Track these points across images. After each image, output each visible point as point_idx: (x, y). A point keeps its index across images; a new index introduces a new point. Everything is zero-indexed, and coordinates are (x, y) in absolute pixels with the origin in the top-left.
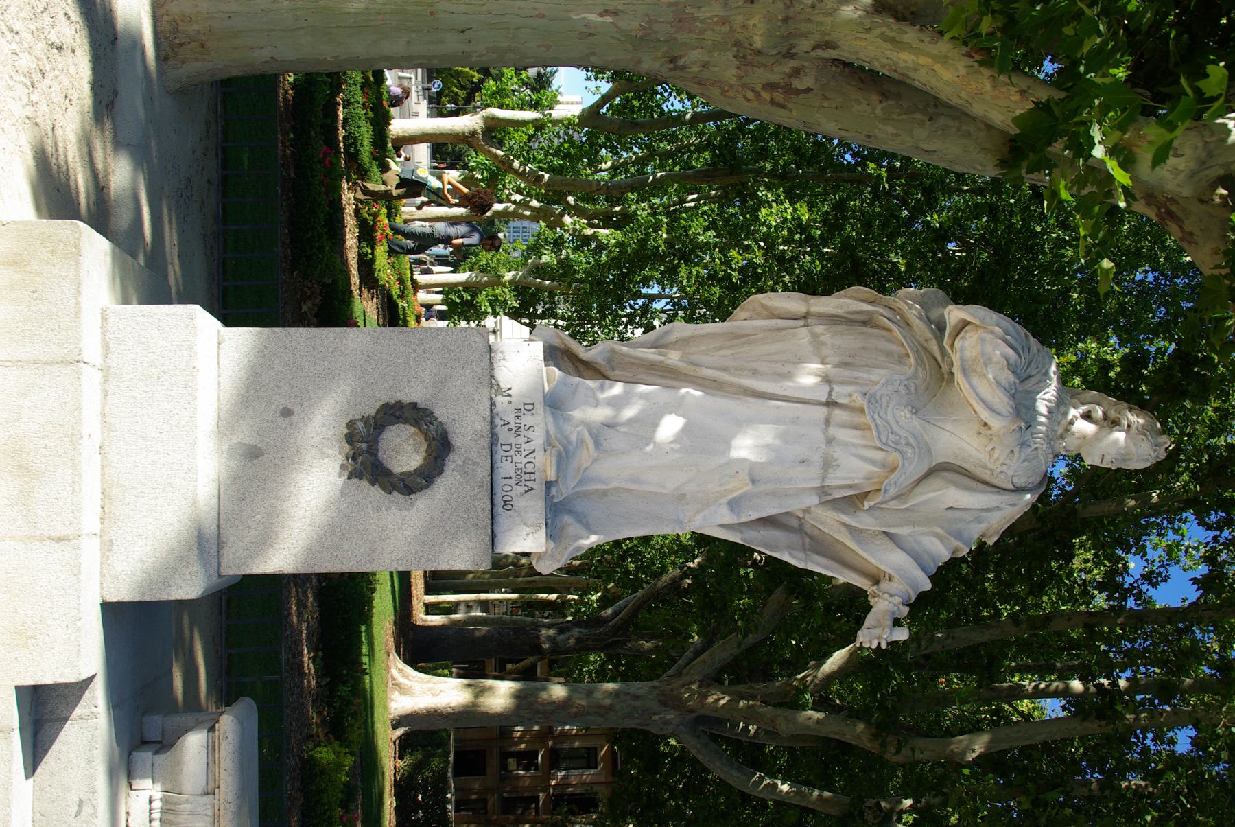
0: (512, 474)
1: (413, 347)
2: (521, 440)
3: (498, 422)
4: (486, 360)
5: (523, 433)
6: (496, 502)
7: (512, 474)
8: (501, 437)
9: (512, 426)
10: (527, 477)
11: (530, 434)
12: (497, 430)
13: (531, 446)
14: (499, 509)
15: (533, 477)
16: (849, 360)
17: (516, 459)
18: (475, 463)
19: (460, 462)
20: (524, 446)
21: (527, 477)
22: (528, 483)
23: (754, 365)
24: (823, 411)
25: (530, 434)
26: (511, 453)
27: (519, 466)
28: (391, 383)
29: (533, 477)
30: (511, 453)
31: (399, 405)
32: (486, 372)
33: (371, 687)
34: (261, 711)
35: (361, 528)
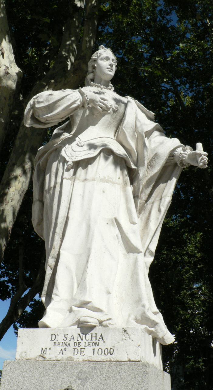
0: (92, 348)
2: (72, 343)
5: (68, 341)
7: (92, 348)
9: (63, 348)
11: (69, 337)
14: (113, 357)
15: (94, 335)
17: (83, 346)
19: (79, 382)
22: (98, 338)
26: (79, 348)
27: (87, 344)
30: (79, 348)
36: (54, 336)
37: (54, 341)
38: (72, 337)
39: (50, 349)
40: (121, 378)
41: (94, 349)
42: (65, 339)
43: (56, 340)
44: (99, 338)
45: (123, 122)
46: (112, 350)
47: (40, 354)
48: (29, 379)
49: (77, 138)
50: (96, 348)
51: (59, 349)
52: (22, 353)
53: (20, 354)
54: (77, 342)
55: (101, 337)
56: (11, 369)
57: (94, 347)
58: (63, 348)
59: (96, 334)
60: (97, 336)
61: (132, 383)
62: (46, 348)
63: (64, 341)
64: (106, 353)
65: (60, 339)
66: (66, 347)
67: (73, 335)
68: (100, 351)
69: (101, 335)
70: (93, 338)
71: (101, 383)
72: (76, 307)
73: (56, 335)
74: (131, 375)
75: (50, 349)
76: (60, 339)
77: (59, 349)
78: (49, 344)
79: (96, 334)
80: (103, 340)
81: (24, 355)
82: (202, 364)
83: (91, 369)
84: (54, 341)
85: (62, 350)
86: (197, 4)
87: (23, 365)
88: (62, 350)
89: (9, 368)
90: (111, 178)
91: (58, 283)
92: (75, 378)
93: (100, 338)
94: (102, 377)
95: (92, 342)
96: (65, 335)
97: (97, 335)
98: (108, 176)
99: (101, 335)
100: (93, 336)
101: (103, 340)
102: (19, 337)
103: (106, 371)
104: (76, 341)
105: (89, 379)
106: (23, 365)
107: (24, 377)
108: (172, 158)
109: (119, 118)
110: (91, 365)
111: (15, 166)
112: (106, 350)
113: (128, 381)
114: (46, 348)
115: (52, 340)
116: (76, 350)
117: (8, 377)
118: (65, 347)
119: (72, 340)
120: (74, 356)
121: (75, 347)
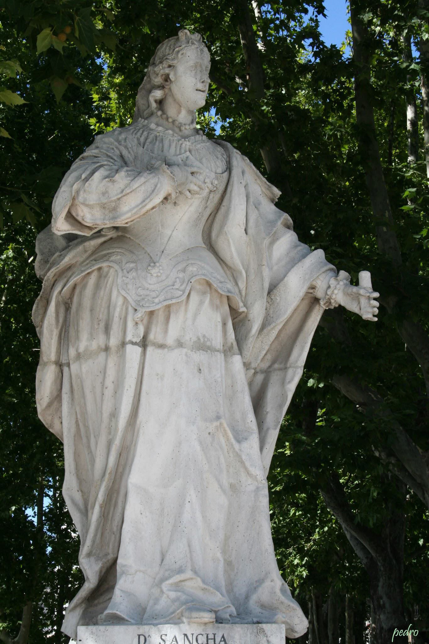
23: (106, 415)
24: (150, 349)
38: (174, 640)
44: (220, 640)
45: (205, 238)
55: (222, 640)
59: (214, 635)
60: (216, 638)
67: (175, 637)
69: (223, 637)
70: (209, 641)
72: (300, 260)
73: (147, 637)
79: (214, 635)
82: (332, 85)
86: (373, 453)
90: (208, 340)
93: (221, 641)
96: (161, 636)
97: (216, 636)
98: (204, 336)
99: (223, 637)
100: (209, 638)
102: (80, 640)
108: (311, 291)
109: (251, 200)
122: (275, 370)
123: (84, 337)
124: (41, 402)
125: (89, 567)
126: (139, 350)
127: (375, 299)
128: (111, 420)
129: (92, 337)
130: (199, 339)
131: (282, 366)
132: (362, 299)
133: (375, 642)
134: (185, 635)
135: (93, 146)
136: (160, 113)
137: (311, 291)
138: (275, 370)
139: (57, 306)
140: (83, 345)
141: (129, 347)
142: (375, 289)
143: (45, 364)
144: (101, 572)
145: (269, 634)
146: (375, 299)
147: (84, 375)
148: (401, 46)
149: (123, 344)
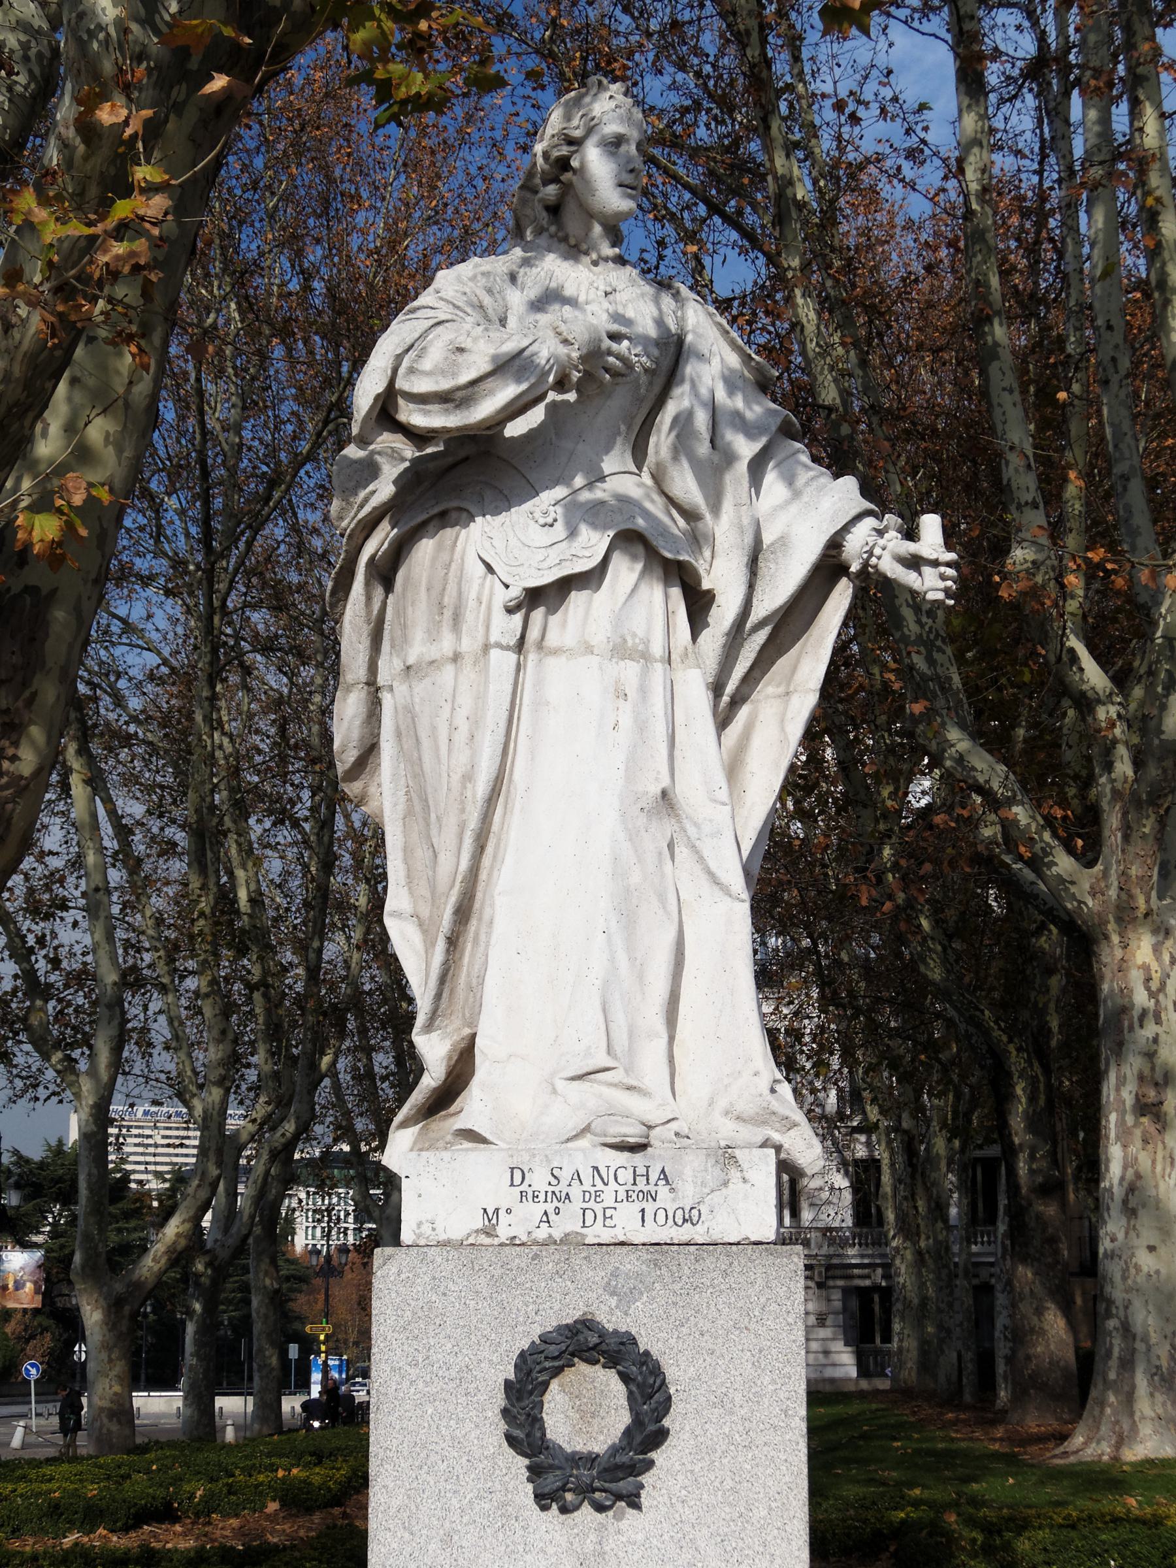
0: (637, 1206)
1: (406, 1384)
2: (576, 1191)
3: (542, 1234)
4: (432, 1252)
5: (563, 1188)
6: (685, 1238)
7: (637, 1206)
8: (569, 1228)
9: (550, 1207)
10: (641, 1181)
11: (566, 1176)
12: (557, 1235)
13: (587, 1174)
14: (698, 1233)
15: (641, 1170)
16: (448, 614)
17: (609, 1200)
18: (615, 1274)
19: (613, 1301)
20: (587, 1186)
21: (641, 1181)
22: (654, 1177)
23: (456, 778)
24: (532, 657)
25: (566, 1176)
27: (622, 1195)
28: (469, 1425)
29: (641, 1170)
31: (659, 1437)
32: (453, 1253)
33: (490, 875)
34: (855, 597)
35: (729, 1483)
36: (517, 1174)
37: (522, 1188)
39: (509, 1211)
40: (730, 1288)
41: (643, 1210)
42: (554, 1182)
43: (526, 1183)
46: (695, 1212)
47: (480, 1226)
48: (459, 1298)
49: (57, 1428)
50: (650, 1207)
51: (536, 1210)
52: (419, 1224)
53: (414, 1227)
54: (592, 1190)
56: (399, 1273)
57: (644, 1205)
58: (550, 1207)
61: (763, 1300)
62: (497, 1210)
63: (551, 1189)
64: (680, 1222)
65: (539, 1180)
66: (560, 1205)
68: (661, 1213)
69: (663, 1171)
71: (675, 1304)
74: (759, 1281)
75: (509, 1211)
76: (539, 1180)
77: (536, 1210)
78: (507, 1197)
80: (668, 1183)
81: (426, 1229)
83: (644, 1267)
84: (522, 1188)
85: (546, 1213)
87: (439, 1260)
88: (546, 1213)
89: (394, 1270)
91: (444, 1063)
92: (600, 1291)
94: (677, 1287)
95: (637, 1189)
99: (663, 1171)
101: (668, 1183)
103: (687, 1271)
104: (587, 1186)
105: (641, 1293)
106: (439, 1260)
107: (444, 1294)
110: (646, 1257)
111: (150, 1286)
112: (680, 1212)
113: (749, 1297)
114: (497, 1210)
115: (512, 1185)
116: (589, 1214)
117: (394, 1295)
118: (556, 1203)
119: (576, 1183)
120: (584, 1231)
121: (585, 1205)
122: (768, 697)
123: (418, 635)
124: (344, 756)
125: (434, 1049)
126: (512, 657)
127: (948, 564)
128: (465, 787)
129: (433, 636)
130: (625, 641)
131: (781, 690)
132: (922, 557)
133: (5, 780)
134: (596, 1168)
135: (430, 289)
136: (553, 229)
137: (833, 553)
138: (768, 697)
139: (368, 584)
140: (417, 651)
141: (495, 653)
142: (949, 546)
143: (348, 690)
144: (450, 1058)
145: (745, 1166)
146: (948, 564)
147: (417, 708)
148: (982, 42)
149: (486, 648)
